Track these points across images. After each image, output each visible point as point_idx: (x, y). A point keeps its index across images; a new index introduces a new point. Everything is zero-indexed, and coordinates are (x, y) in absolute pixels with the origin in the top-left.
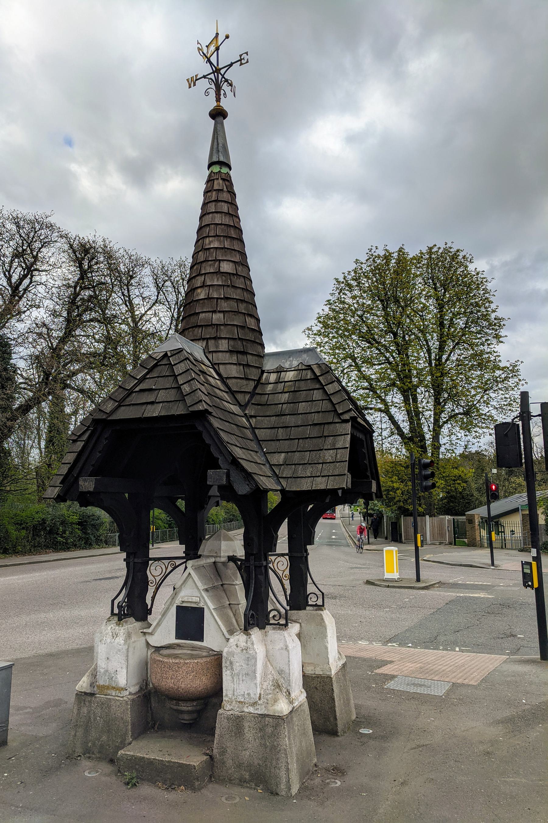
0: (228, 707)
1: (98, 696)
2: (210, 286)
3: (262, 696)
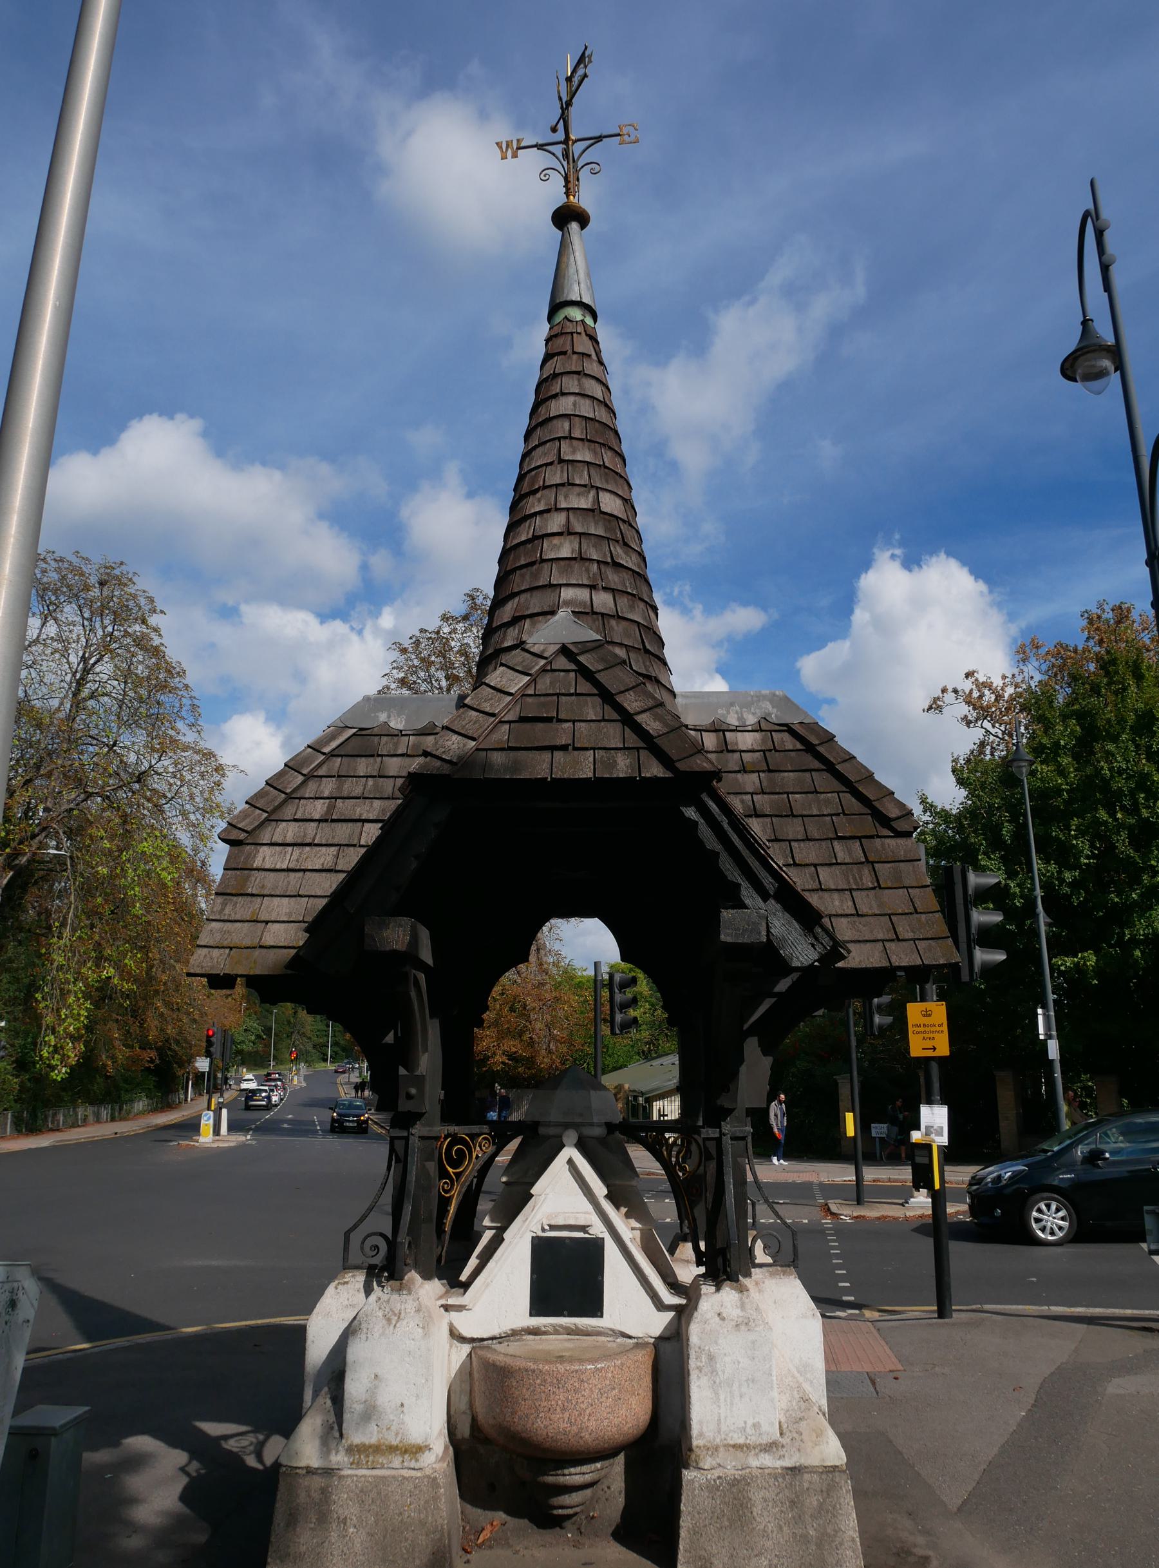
0: (707, 1463)
1: (349, 1472)
2: (580, 534)
3: (785, 1426)
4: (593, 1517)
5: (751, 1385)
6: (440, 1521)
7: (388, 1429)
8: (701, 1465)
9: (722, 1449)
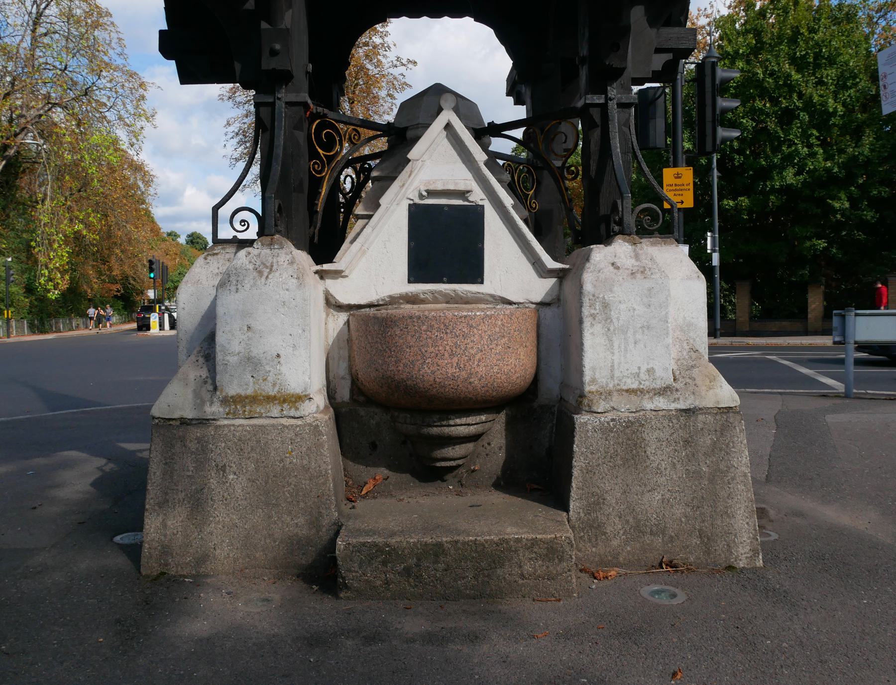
1: (226, 422)
3: (677, 373)
4: (473, 471)
5: (646, 331)
6: (324, 466)
7: (265, 380)
8: (595, 408)
9: (615, 394)
